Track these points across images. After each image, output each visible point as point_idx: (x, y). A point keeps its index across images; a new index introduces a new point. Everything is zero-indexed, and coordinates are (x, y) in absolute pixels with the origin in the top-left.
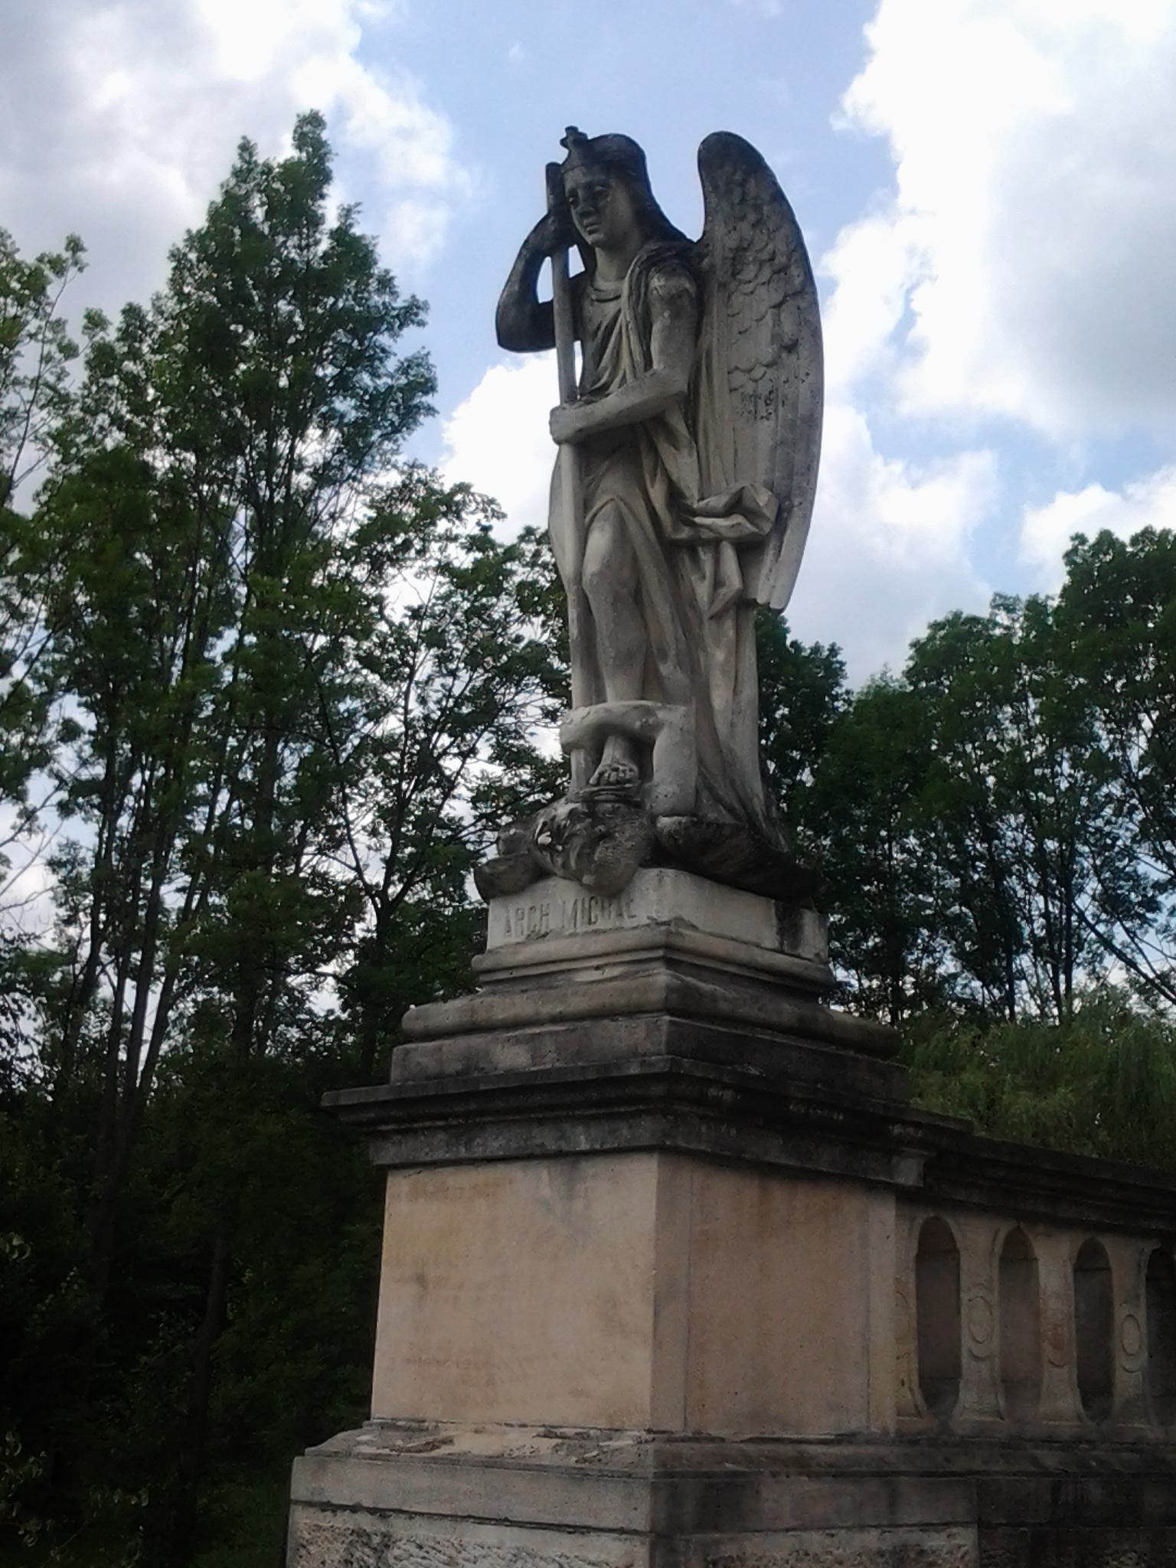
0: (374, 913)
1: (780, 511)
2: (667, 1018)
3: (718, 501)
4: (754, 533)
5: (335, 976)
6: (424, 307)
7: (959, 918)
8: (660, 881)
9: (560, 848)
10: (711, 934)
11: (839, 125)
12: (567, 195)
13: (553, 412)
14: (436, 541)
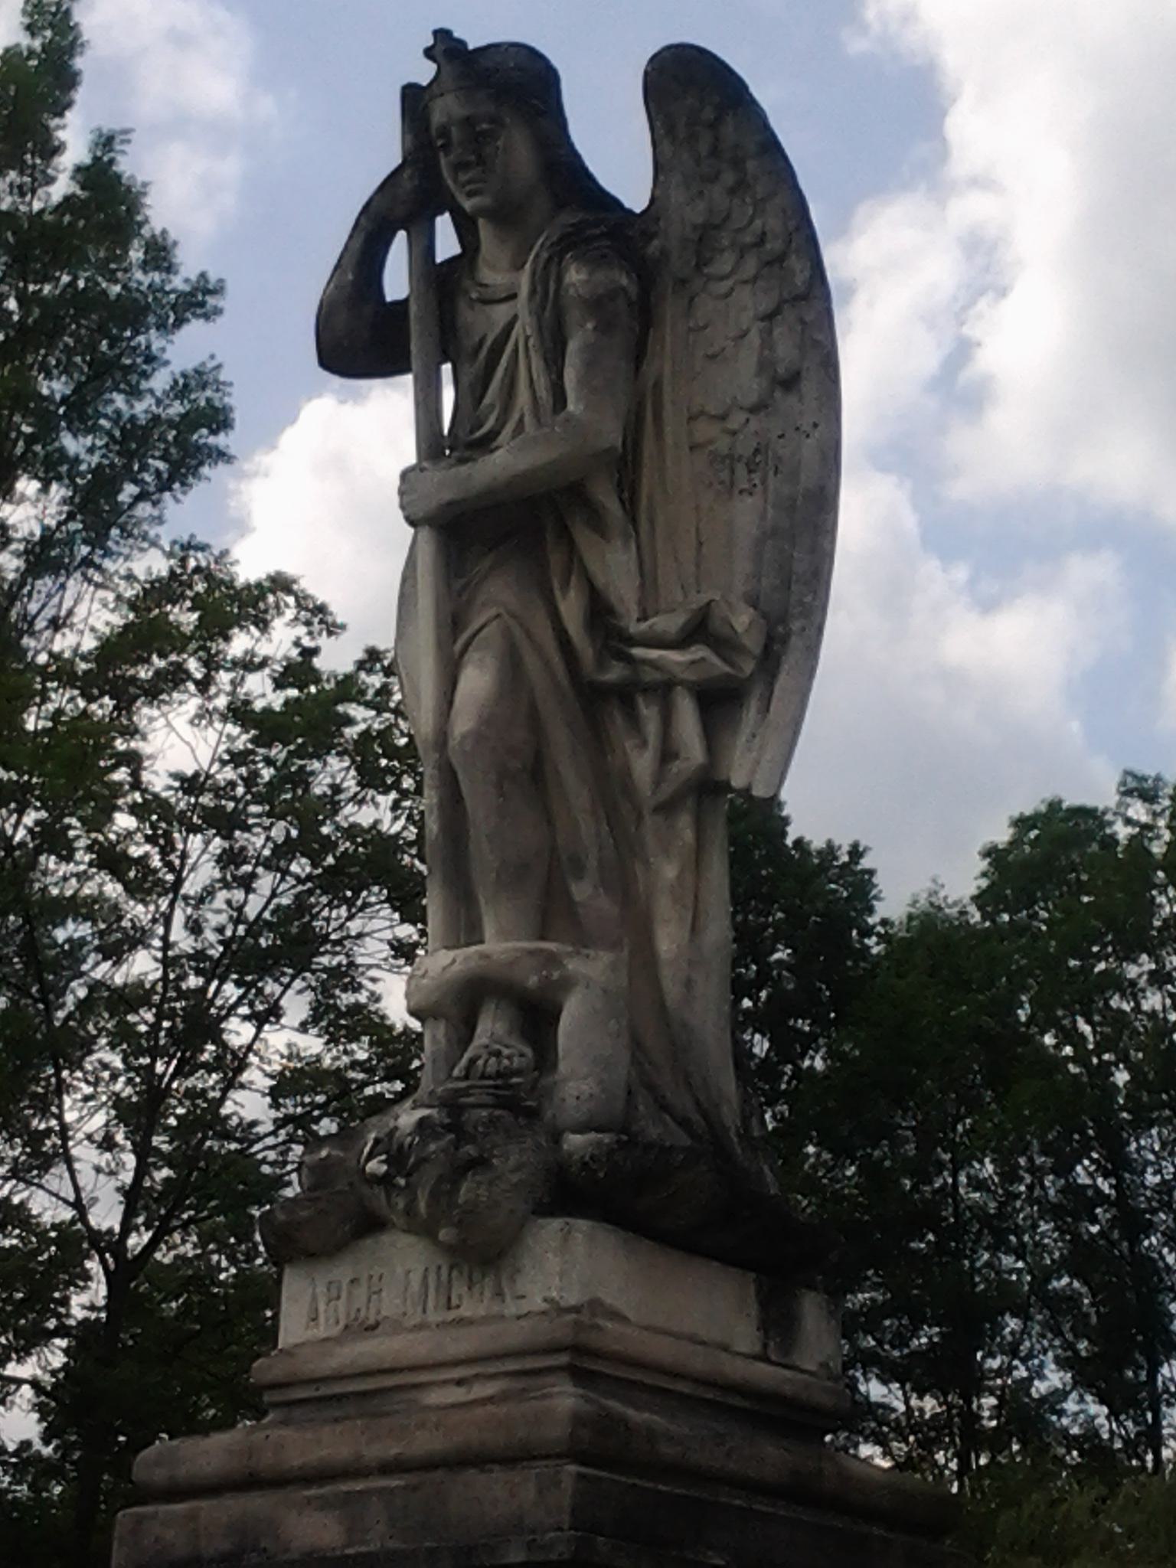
0: (103, 1279)
1: (767, 648)
2: (573, 1468)
3: (670, 623)
4: (728, 675)
5: (35, 1383)
6: (218, 290)
7: (1071, 1299)
8: (565, 1240)
9: (402, 1182)
10: (647, 1328)
11: (857, 46)
12: (434, 133)
13: (405, 475)
14: (228, 670)
